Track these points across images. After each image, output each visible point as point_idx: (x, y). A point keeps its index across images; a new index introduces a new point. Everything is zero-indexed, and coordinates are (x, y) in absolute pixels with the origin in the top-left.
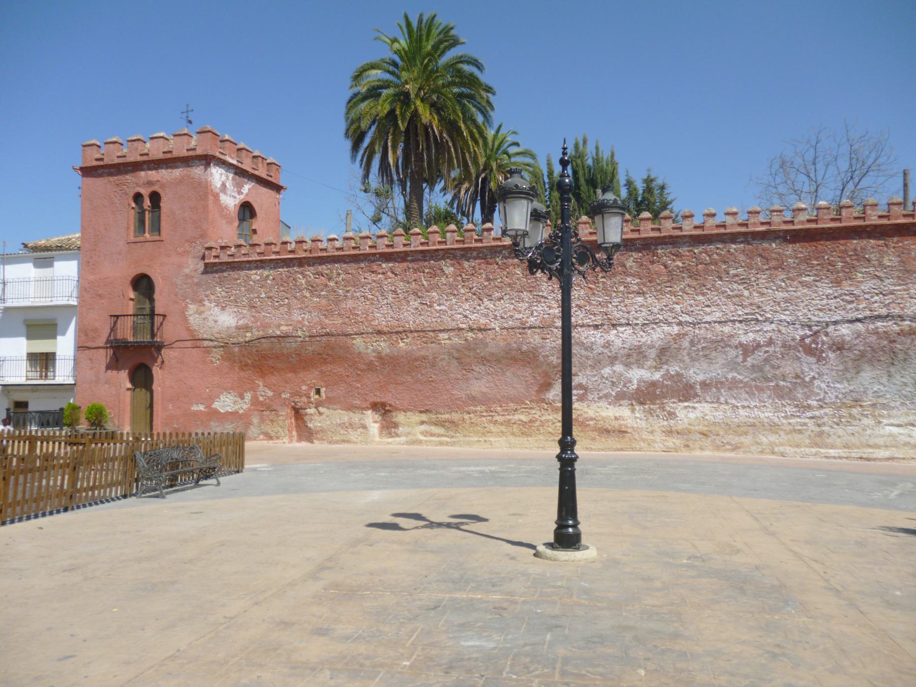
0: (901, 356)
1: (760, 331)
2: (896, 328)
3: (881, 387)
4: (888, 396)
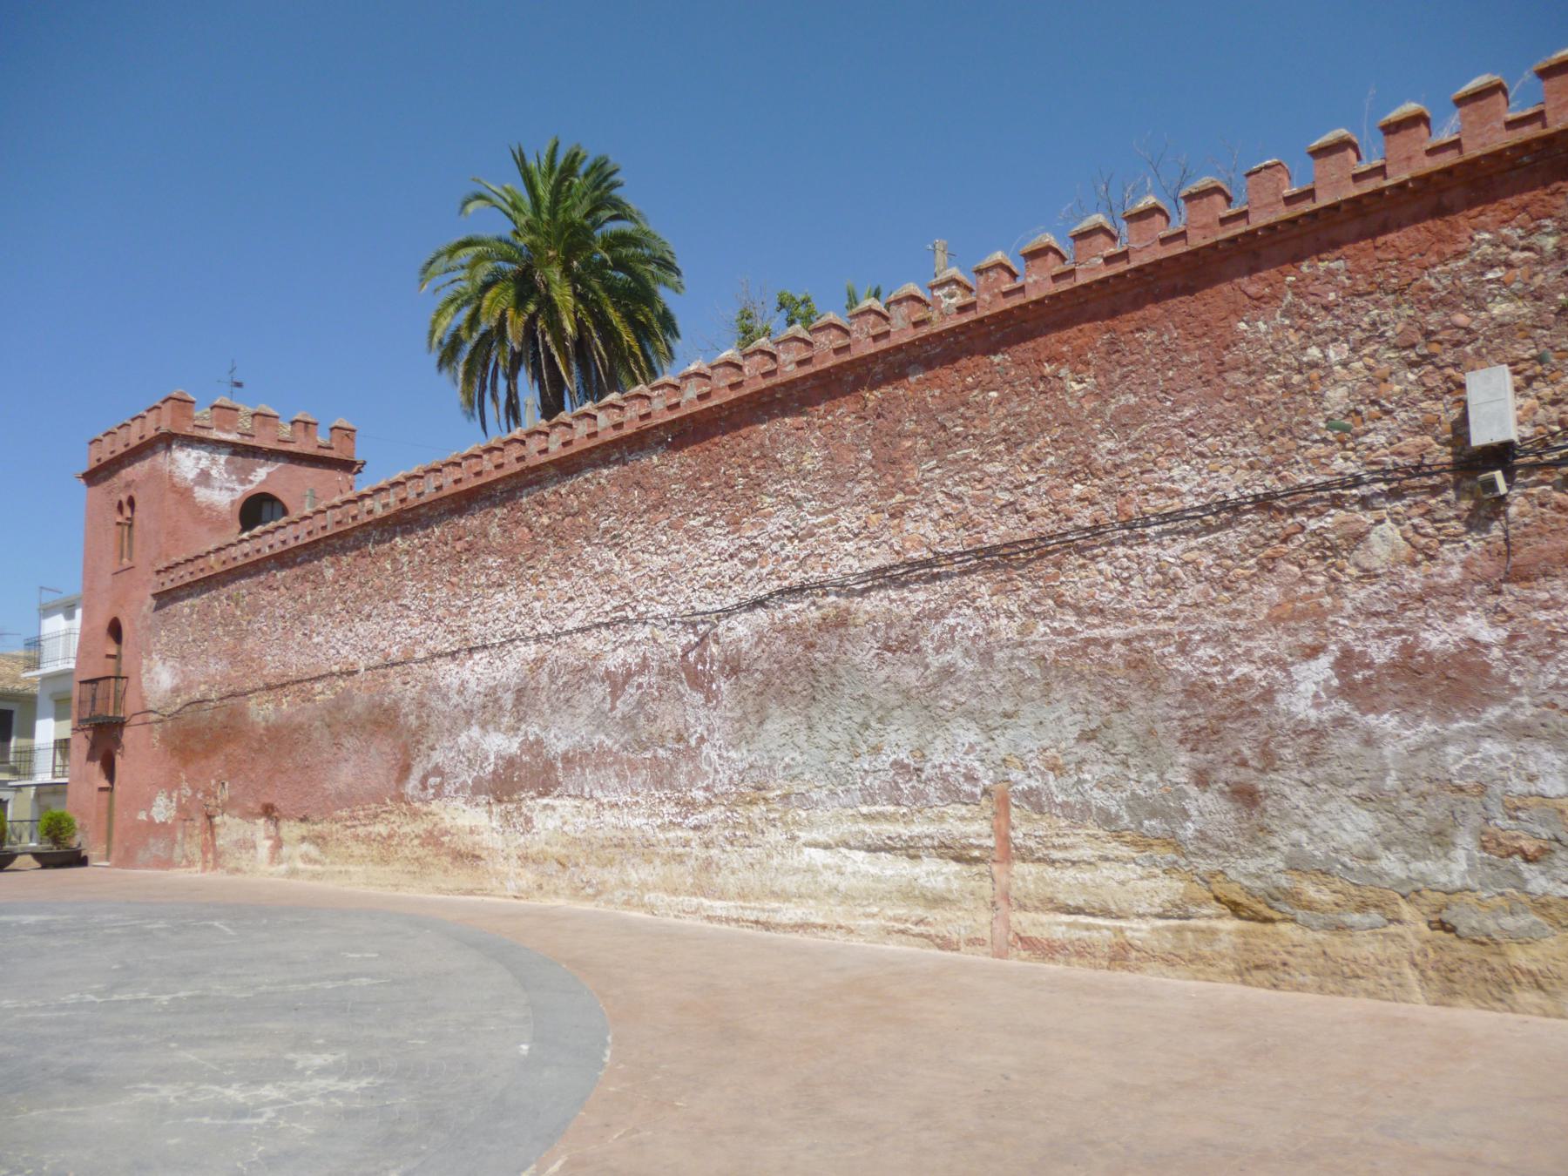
0: (825, 680)
1: (630, 642)
2: (815, 614)
3: (796, 755)
4: (807, 776)
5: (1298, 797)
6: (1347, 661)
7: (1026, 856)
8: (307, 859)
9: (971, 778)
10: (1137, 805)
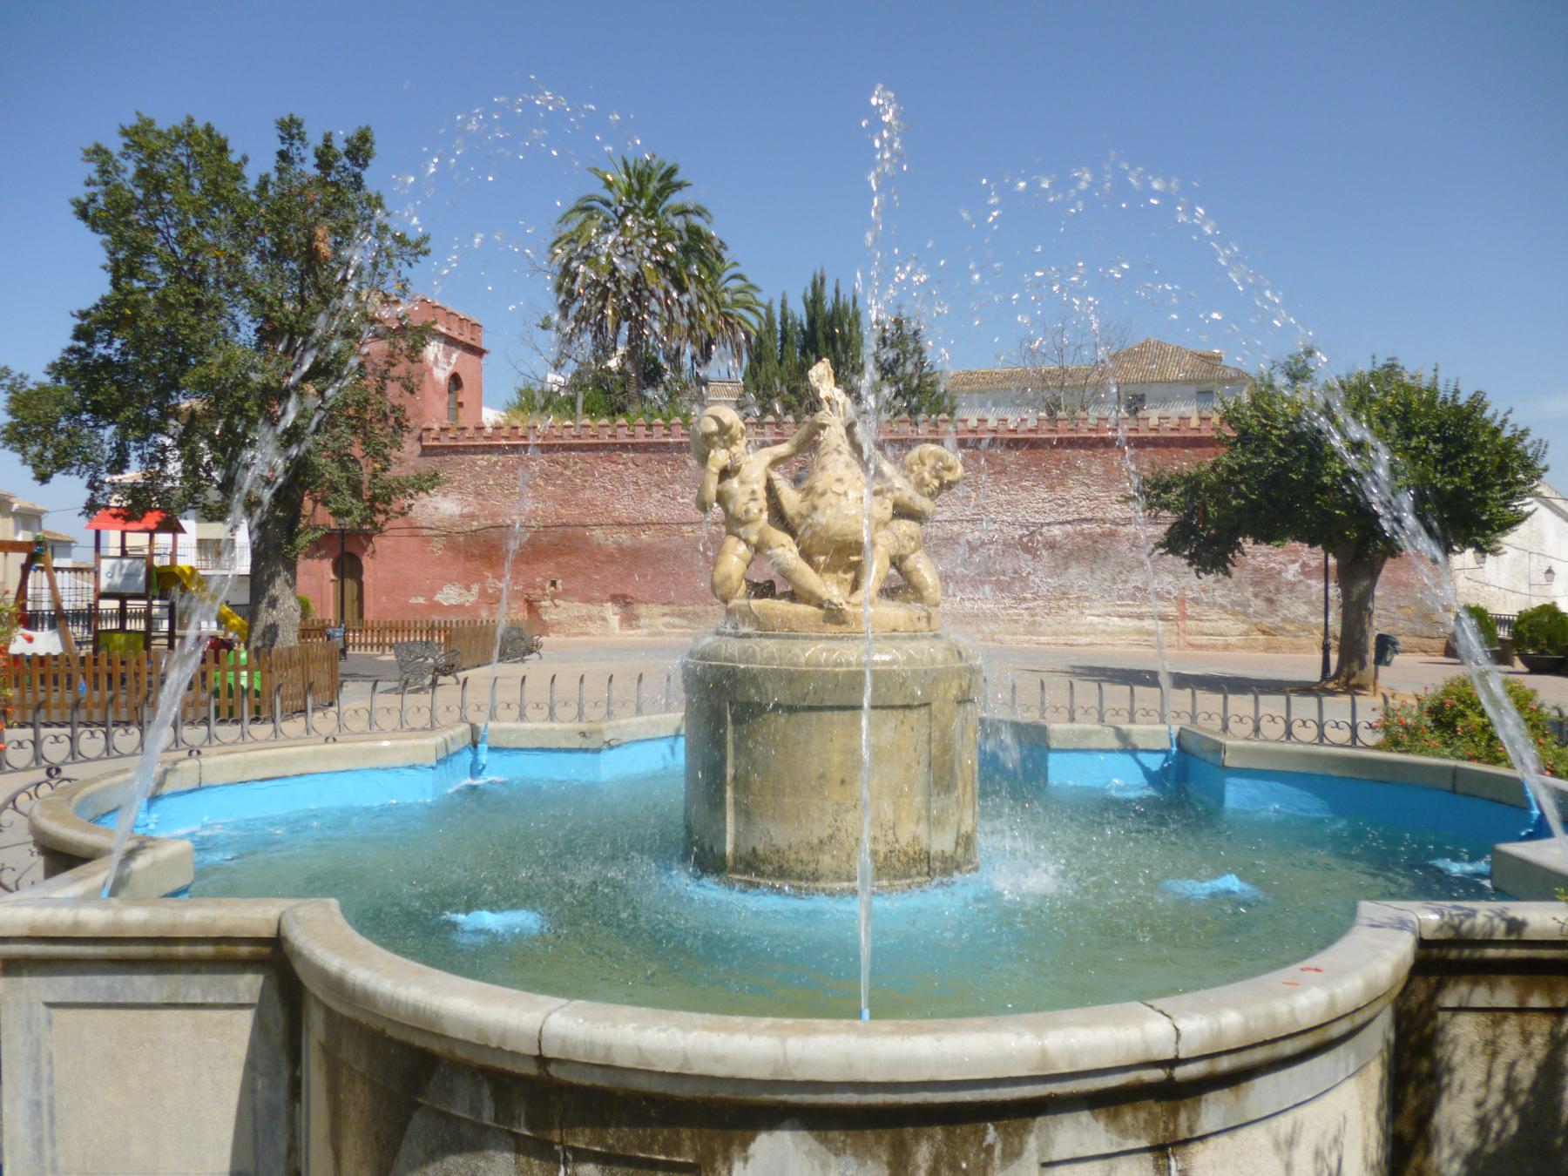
5: (1286, 601)
6: (1304, 565)
7: (1191, 618)
8: (667, 625)
9: (1169, 593)
10: (1233, 603)
